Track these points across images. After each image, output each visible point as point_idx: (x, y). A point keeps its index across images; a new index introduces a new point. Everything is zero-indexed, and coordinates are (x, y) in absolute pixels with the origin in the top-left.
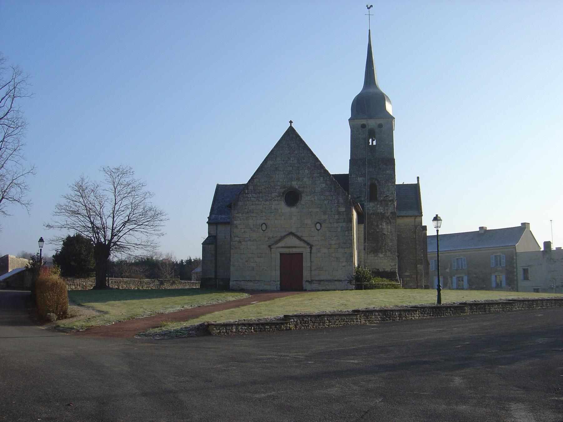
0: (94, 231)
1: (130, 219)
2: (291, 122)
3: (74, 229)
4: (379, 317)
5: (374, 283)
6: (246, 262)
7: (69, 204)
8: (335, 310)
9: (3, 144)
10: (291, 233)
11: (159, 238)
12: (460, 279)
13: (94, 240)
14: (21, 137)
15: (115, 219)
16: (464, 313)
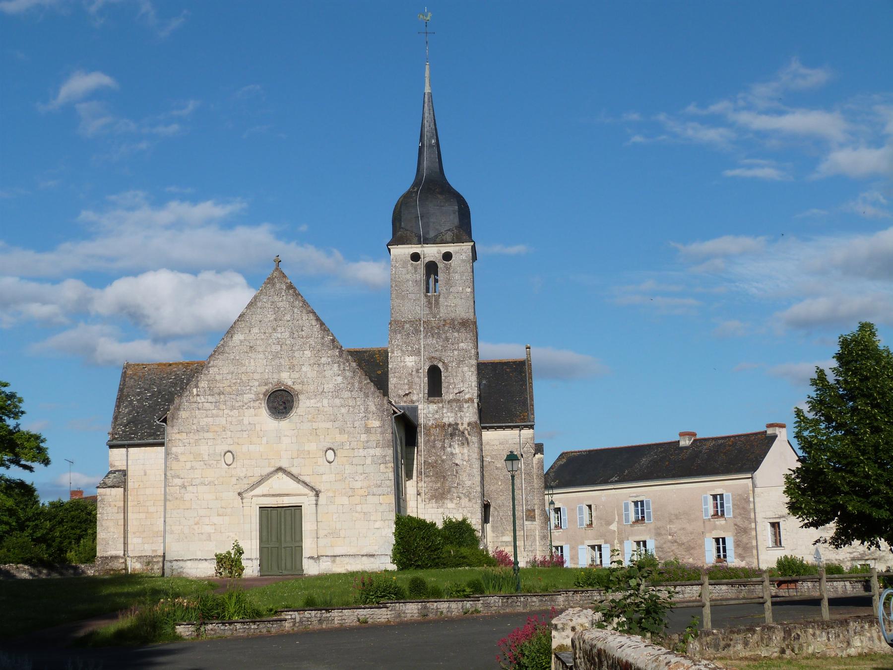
6: (196, 524)
10: (280, 469)
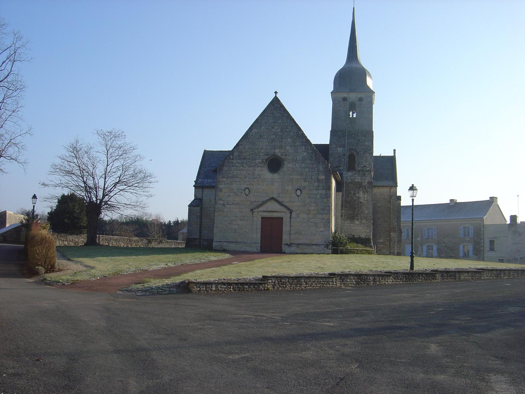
0: (86, 191)
1: (121, 180)
2: (276, 93)
3: (68, 188)
4: (354, 280)
5: (349, 248)
7: (64, 164)
8: (312, 272)
9: (2, 106)
10: (273, 199)
11: (148, 199)
12: (430, 248)
13: (86, 199)
14: (20, 99)
15: (106, 180)
16: (436, 279)
